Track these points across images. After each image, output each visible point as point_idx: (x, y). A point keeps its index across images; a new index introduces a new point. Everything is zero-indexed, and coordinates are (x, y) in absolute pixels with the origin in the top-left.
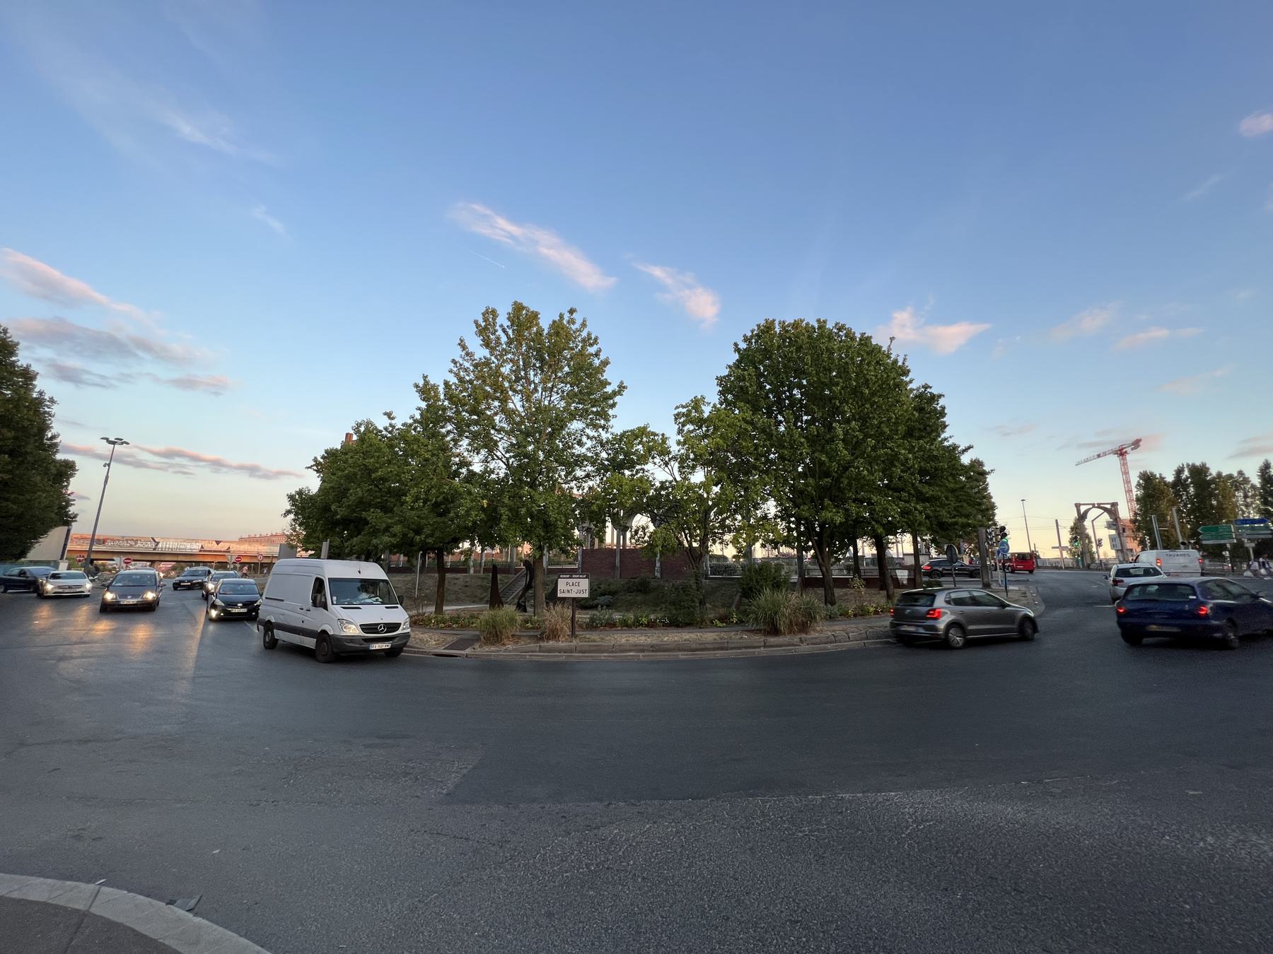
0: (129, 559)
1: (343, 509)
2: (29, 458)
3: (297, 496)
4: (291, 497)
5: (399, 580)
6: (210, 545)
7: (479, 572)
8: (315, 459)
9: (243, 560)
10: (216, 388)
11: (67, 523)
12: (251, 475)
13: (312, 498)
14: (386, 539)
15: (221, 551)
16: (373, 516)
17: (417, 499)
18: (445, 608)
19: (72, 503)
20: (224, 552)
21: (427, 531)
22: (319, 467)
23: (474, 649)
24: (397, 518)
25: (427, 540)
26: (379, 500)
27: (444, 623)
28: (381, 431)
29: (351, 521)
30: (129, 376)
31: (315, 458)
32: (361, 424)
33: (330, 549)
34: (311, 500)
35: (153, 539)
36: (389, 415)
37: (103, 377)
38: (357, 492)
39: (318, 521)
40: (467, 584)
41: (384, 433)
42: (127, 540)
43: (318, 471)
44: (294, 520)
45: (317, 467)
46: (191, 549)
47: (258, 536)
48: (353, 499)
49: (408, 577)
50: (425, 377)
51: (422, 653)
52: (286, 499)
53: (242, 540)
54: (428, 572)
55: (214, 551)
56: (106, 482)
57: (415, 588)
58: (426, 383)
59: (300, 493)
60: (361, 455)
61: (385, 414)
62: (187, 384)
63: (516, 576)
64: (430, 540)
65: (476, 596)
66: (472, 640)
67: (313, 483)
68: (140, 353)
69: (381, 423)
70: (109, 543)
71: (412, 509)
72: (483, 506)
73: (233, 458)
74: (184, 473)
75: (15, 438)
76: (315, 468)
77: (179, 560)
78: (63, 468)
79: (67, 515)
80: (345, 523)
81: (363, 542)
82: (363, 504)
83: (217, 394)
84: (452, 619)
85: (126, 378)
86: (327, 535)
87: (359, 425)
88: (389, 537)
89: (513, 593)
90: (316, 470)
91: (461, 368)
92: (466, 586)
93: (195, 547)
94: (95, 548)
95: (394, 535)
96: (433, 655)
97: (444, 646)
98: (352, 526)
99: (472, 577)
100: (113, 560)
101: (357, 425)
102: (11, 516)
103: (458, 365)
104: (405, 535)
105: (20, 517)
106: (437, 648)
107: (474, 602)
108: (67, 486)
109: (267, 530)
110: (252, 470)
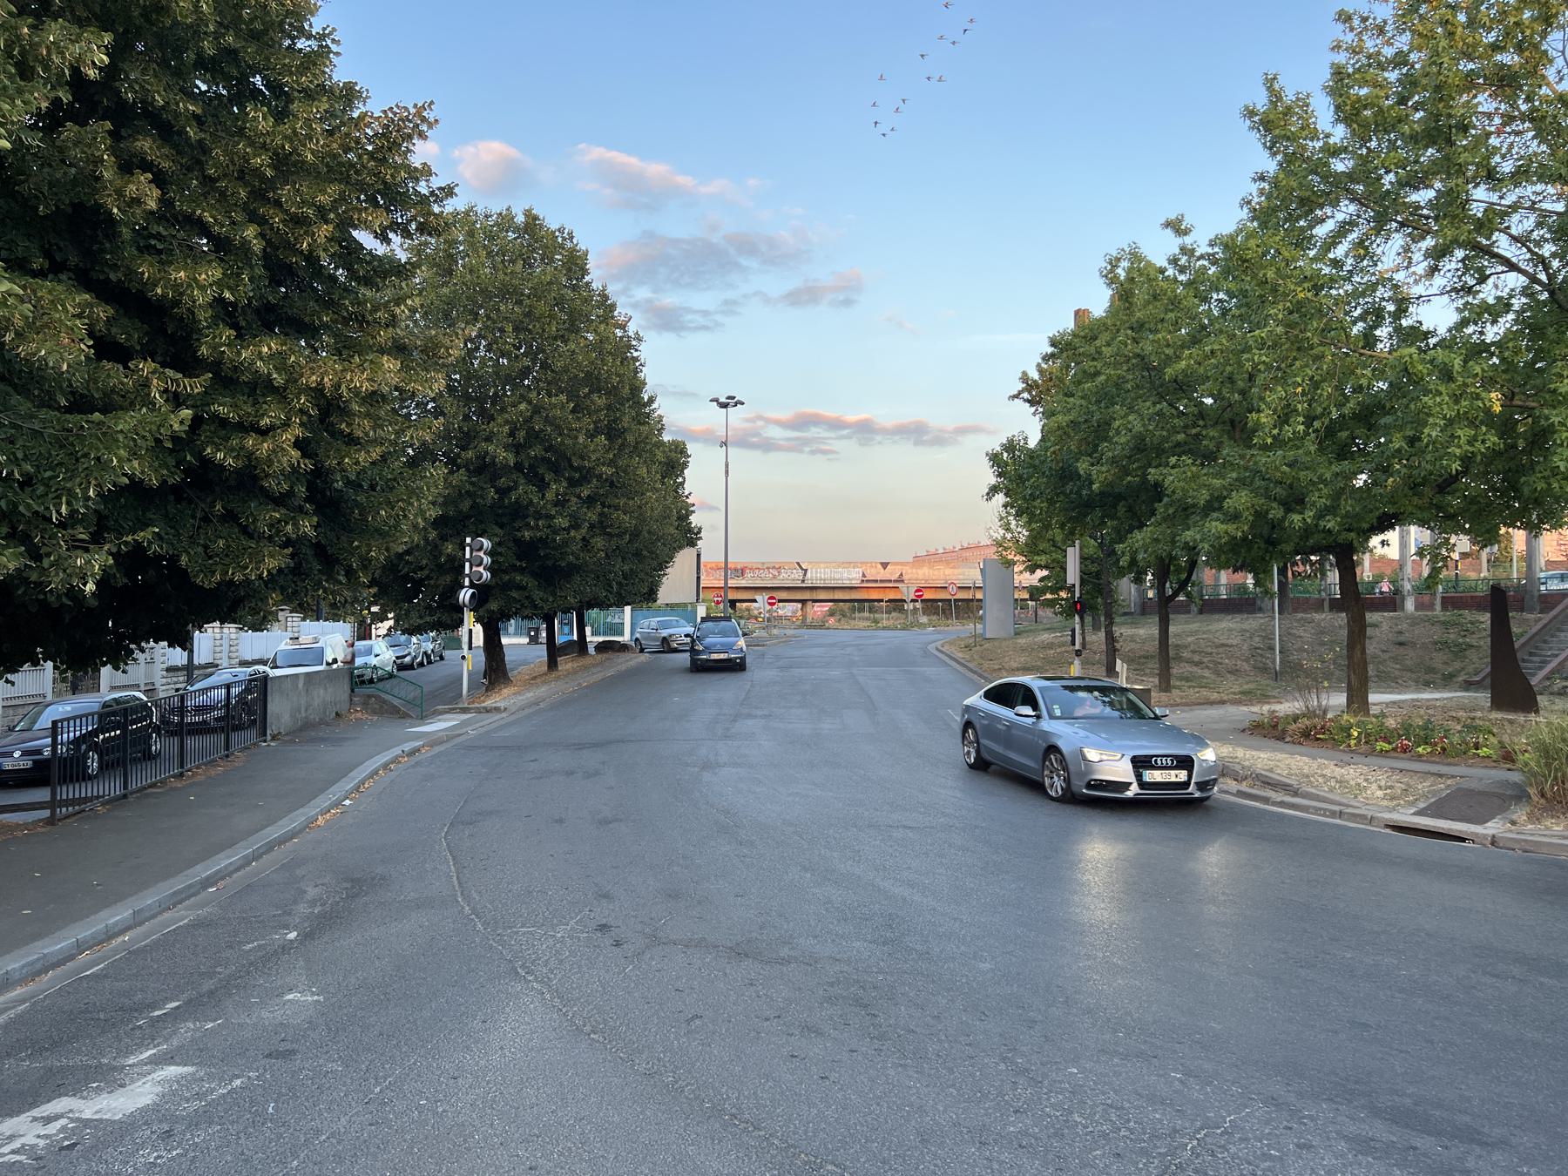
0: (774, 598)
1: (1104, 469)
2: (630, 438)
3: (1005, 455)
4: (995, 458)
5: (1230, 630)
6: (873, 571)
7: (1431, 607)
8: (1024, 378)
9: (928, 595)
10: (846, 293)
11: (692, 543)
12: (917, 443)
13: (1031, 454)
14: (1216, 526)
15: (890, 581)
16: (1175, 476)
17: (1284, 418)
18: (1373, 698)
19: (692, 509)
20: (895, 581)
21: (1318, 498)
22: (1035, 393)
23: (1513, 823)
24: (1234, 475)
25: (1322, 523)
26: (1181, 437)
27: (1386, 740)
28: (1162, 271)
29: (1120, 497)
30: (734, 302)
31: (1024, 373)
32: (1118, 260)
33: (1081, 563)
34: (1032, 457)
35: (798, 563)
36: (1177, 227)
37: (706, 313)
38: (1130, 423)
39: (1051, 502)
40: (1401, 639)
41: (1170, 272)
42: (768, 568)
43: (1031, 402)
44: (1005, 506)
45: (1030, 393)
46: (849, 579)
47: (941, 551)
48: (1123, 440)
49: (1252, 623)
50: (1270, 82)
51: (1355, 817)
52: (986, 463)
53: (918, 560)
54: (1295, 610)
55: (882, 581)
56: (727, 472)
57: (1272, 648)
58: (1275, 95)
59: (1010, 446)
60: (1129, 332)
61: (1168, 224)
62: (804, 296)
63: (1546, 618)
64: (1331, 523)
65: (1431, 670)
66: (1501, 797)
67: (1029, 427)
68: (744, 261)
69: (1160, 250)
70: (749, 574)
71: (1278, 442)
72: (1488, 411)
73: (885, 414)
74: (825, 452)
75: (609, 407)
76: (1026, 395)
77: (836, 597)
78: (673, 454)
79: (690, 530)
80: (1109, 500)
81: (1157, 540)
82: (1146, 451)
83: (848, 303)
84: (1407, 728)
85: (730, 307)
86: (1072, 533)
87: (1114, 263)
88: (1222, 523)
89: (1546, 662)
90: (1028, 401)
91: (1366, 29)
92: (1401, 644)
93: (851, 576)
94: (732, 583)
95: (1235, 517)
96: (1388, 826)
97: (1412, 804)
98: (1122, 509)
99: (1415, 621)
100: (755, 601)
101: (1111, 263)
102: (625, 533)
103: (1356, 22)
104: (1260, 515)
105: (635, 534)
106: (1393, 809)
107: (1427, 684)
108: (682, 483)
109: (953, 541)
110: (916, 433)
